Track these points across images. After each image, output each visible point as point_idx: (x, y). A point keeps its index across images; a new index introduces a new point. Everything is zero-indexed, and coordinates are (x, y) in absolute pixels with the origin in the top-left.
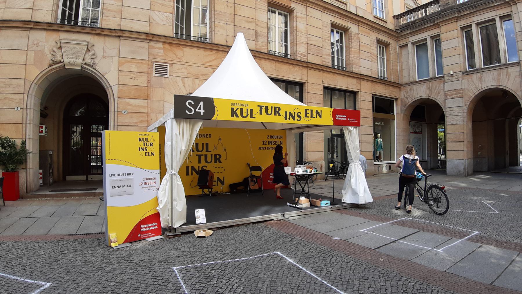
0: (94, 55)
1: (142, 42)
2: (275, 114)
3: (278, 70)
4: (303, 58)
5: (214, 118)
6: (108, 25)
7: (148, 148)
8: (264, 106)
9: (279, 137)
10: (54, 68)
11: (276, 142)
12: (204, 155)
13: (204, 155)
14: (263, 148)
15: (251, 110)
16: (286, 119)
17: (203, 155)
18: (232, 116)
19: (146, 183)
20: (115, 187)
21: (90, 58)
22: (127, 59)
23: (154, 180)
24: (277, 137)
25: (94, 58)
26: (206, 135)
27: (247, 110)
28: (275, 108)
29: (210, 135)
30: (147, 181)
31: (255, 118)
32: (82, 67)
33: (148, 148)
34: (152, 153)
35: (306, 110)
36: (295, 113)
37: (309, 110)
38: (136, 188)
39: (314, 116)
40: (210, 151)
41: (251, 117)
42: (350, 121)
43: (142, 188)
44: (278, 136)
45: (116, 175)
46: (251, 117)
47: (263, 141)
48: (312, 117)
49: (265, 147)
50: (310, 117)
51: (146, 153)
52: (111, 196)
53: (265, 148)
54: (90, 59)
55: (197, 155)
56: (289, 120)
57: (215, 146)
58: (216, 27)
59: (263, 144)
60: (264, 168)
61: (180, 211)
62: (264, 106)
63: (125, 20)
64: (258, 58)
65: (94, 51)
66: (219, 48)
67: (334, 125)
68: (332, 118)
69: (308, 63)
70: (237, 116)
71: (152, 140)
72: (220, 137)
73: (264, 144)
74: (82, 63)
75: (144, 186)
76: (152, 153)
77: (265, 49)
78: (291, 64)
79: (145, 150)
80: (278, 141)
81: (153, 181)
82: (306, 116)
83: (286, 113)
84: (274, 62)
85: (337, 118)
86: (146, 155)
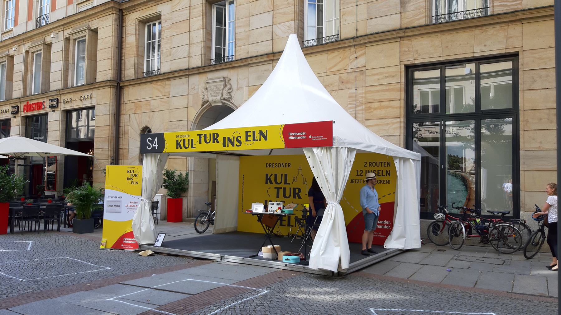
0: (230, 89)
1: (266, 65)
2: (214, 142)
3: (447, 47)
4: (512, 5)
5: (164, 152)
6: (240, 55)
7: (134, 178)
8: (203, 135)
9: (384, 164)
10: (205, 108)
11: (379, 172)
12: (282, 188)
13: (282, 188)
14: (357, 181)
15: (192, 140)
16: (224, 146)
17: (281, 188)
18: (177, 148)
19: (130, 206)
20: (110, 206)
21: (227, 92)
22: (254, 87)
23: (137, 204)
24: (380, 163)
25: (231, 92)
26: (285, 164)
27: (189, 140)
28: (214, 134)
29: (289, 164)
30: (131, 204)
31: (195, 148)
32: (223, 103)
33: (134, 178)
34: (136, 182)
35: (247, 133)
36: (234, 137)
37: (250, 132)
38: (123, 208)
39: (258, 138)
40: (289, 184)
41: (192, 147)
42: (313, 140)
43: (127, 209)
44: (382, 162)
45: (111, 197)
46: (192, 147)
47: (358, 171)
48: (254, 140)
49: (361, 180)
50: (252, 140)
51: (132, 182)
52: (107, 212)
53: (360, 182)
54: (227, 93)
55: (275, 188)
56: (228, 146)
57: (294, 177)
58: (343, 15)
59: (358, 175)
60: (357, 211)
61: (144, 231)
62: (203, 135)
63: (252, 45)
64: (405, 39)
65: (231, 85)
66: (343, 44)
67: (285, 148)
68: (283, 139)
69: (516, 13)
70: (181, 148)
71: (137, 171)
72: (300, 166)
73: (359, 174)
74: (221, 100)
75: (128, 207)
76: (136, 182)
77: (419, 19)
78: (476, 27)
79: (131, 179)
80: (382, 171)
81: (135, 204)
82: (247, 140)
83: (224, 138)
84: (439, 35)
85: (290, 138)
86: (132, 184)
